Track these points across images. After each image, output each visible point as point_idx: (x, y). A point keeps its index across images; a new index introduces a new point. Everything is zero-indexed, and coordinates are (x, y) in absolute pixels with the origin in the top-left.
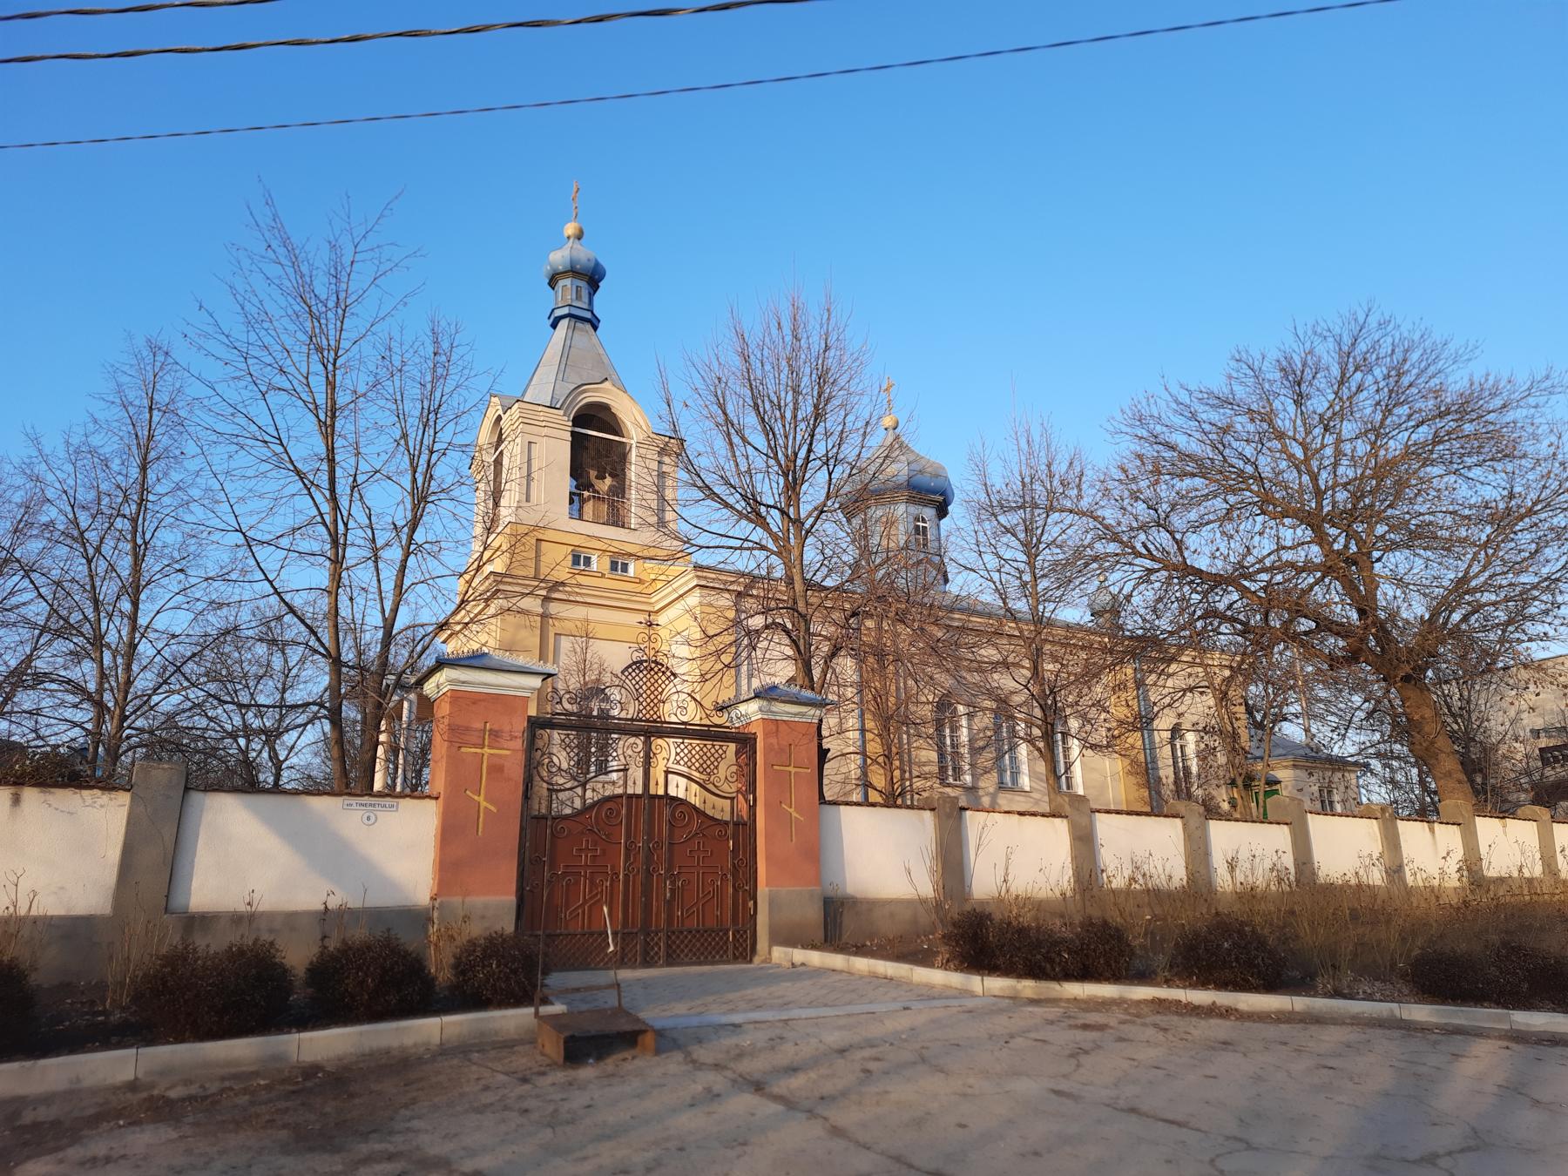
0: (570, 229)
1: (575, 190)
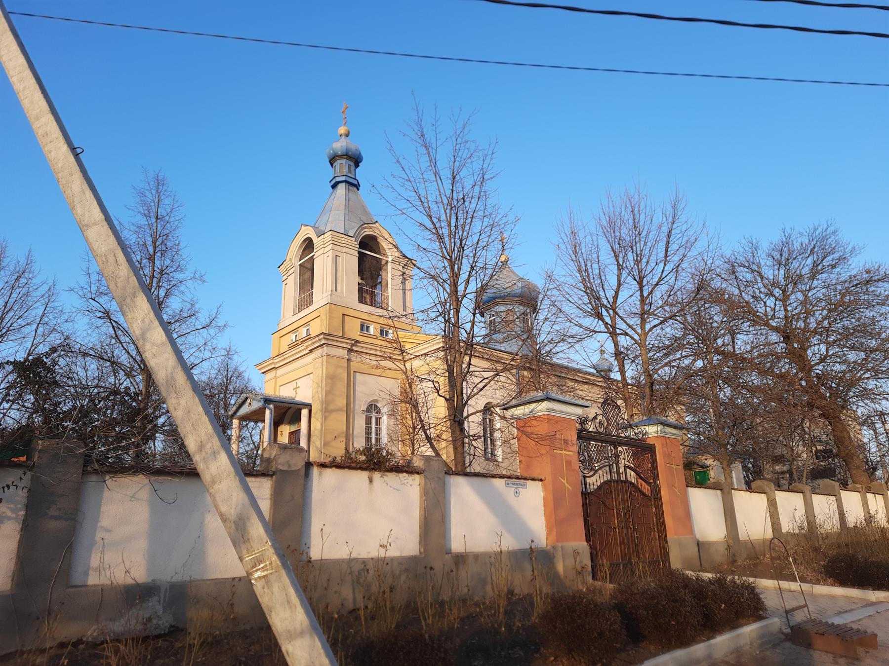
0: (342, 130)
1: (344, 107)
